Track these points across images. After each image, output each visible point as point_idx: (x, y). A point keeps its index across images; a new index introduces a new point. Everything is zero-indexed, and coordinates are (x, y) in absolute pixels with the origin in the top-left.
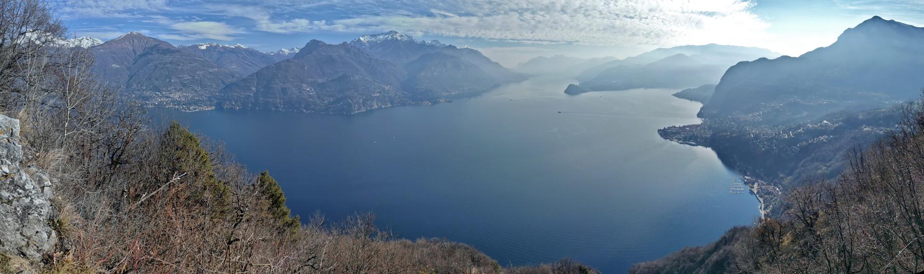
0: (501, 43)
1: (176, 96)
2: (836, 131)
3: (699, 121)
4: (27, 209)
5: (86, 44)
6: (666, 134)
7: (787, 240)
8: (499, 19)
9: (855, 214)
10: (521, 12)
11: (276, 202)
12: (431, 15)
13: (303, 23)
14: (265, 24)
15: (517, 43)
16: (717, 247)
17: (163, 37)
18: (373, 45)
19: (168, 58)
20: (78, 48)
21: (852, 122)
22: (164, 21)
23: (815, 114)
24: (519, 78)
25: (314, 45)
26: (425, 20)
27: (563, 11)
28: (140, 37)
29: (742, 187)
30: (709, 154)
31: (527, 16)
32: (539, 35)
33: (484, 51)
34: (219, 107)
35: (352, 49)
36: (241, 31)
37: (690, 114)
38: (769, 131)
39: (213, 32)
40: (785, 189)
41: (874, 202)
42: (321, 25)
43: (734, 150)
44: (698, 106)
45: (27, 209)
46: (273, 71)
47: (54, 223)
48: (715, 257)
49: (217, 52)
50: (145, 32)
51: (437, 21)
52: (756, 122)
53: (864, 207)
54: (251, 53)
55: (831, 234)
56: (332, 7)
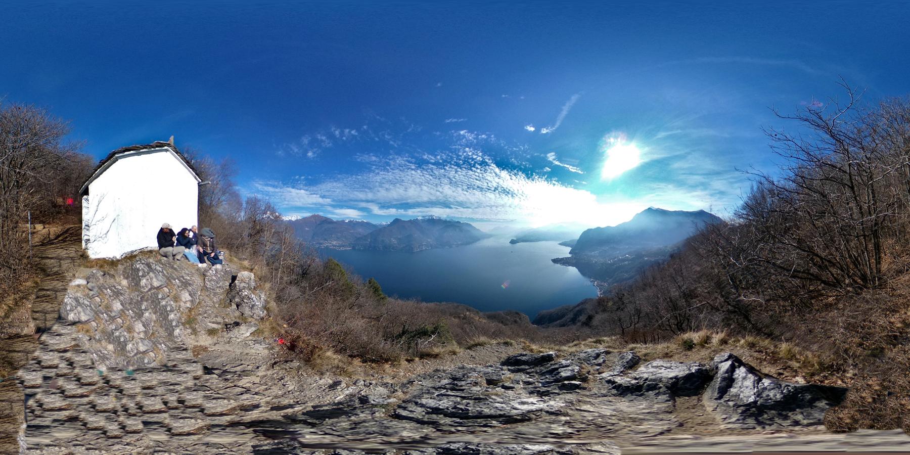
0: (482, 220)
1: (334, 243)
2: (632, 260)
3: (570, 256)
4: (253, 306)
5: (294, 219)
6: (555, 261)
7: (610, 304)
8: (481, 210)
9: (641, 296)
10: (491, 207)
11: (376, 290)
12: (450, 208)
13: (393, 211)
14: (376, 210)
15: (489, 220)
16: (578, 305)
17: (329, 216)
18: (423, 221)
19: (331, 226)
20: (290, 221)
21: (639, 256)
22: (330, 209)
23: (623, 253)
24: (488, 236)
25: (397, 221)
26: (448, 210)
27: (510, 206)
28: (318, 216)
29: (590, 283)
30: (573, 271)
31: (494, 208)
32: (499, 217)
33: (474, 224)
34: (354, 248)
35: (414, 222)
36: (365, 214)
37: (566, 252)
38: (601, 260)
39: (351, 214)
40: (609, 284)
41: (650, 292)
42: (402, 211)
43: (585, 268)
44: (569, 249)
45: (253, 306)
46: (379, 231)
47: (265, 308)
48: (577, 309)
49: (353, 224)
50: (321, 214)
51: (453, 210)
52: (596, 256)
53: (645, 294)
54: (368, 223)
55: (630, 302)
56: (407, 204)
